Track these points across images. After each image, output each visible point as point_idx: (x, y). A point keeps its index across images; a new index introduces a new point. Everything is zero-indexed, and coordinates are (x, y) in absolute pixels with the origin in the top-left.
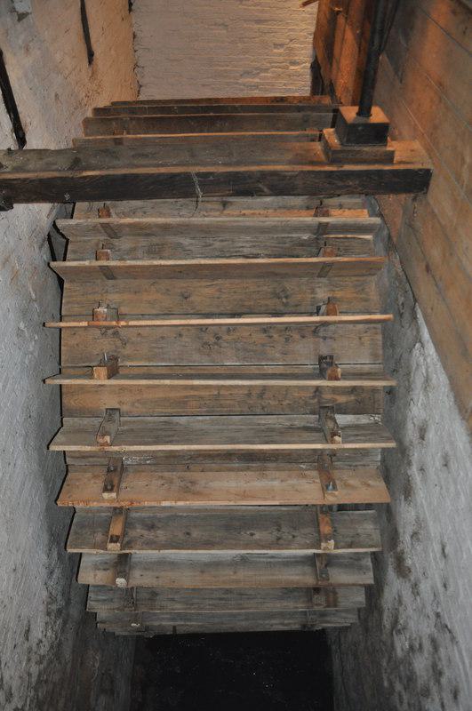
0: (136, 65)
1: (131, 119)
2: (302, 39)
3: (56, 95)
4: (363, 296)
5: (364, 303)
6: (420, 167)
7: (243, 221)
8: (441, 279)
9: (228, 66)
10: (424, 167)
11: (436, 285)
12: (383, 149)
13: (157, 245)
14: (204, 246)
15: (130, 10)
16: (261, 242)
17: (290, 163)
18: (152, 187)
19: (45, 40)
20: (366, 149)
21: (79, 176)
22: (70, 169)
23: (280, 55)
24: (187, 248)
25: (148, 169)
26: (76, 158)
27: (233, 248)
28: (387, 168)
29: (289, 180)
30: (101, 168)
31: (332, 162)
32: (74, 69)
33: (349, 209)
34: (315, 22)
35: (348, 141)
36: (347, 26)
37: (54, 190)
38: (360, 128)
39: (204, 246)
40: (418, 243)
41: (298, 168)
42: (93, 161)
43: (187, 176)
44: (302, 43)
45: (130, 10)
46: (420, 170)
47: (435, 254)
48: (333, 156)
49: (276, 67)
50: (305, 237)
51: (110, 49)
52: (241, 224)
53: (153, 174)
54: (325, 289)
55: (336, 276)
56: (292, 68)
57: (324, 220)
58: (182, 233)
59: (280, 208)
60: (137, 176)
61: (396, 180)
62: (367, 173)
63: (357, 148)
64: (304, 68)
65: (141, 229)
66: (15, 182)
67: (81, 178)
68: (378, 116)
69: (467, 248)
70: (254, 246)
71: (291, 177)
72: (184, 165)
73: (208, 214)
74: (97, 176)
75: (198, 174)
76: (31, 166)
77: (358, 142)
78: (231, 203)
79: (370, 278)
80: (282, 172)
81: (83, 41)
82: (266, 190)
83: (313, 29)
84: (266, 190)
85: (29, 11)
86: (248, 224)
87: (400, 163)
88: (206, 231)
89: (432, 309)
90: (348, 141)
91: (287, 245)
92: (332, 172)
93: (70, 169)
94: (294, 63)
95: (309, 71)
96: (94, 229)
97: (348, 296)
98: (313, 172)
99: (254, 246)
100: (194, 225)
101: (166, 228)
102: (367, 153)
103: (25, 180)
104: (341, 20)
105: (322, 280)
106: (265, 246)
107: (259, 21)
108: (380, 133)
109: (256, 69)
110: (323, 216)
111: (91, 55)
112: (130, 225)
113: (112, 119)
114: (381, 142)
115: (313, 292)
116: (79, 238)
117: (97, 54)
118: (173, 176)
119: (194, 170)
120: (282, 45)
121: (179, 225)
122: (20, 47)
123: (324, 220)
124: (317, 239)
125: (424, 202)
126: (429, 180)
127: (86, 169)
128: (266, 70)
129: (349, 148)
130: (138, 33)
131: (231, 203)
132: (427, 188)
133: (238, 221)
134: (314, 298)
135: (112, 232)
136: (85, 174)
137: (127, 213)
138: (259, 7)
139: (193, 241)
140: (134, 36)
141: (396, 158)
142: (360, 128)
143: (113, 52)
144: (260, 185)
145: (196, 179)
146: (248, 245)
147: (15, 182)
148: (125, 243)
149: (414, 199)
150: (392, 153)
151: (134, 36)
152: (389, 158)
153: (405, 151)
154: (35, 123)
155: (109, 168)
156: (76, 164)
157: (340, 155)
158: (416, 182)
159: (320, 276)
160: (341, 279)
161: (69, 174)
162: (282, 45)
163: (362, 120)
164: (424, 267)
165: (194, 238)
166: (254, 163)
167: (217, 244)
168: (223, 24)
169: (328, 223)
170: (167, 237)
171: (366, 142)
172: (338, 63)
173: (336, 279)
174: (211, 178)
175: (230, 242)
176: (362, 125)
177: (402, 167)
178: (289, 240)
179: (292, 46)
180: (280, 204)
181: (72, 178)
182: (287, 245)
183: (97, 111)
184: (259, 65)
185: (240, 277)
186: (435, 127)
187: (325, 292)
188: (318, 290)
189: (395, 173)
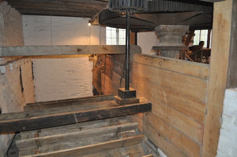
0: (35, 96)
1: (42, 105)
2: (89, 84)
3: (12, 100)
4: (138, 151)
5: (139, 154)
6: (148, 103)
7: (91, 131)
8: (166, 136)
9: (66, 93)
10: (149, 103)
11: (165, 139)
12: (135, 99)
13: (58, 146)
14: (76, 144)
15: (33, 79)
16: (97, 139)
17: (107, 107)
18: (58, 121)
19: (9, 82)
20: (130, 99)
21: (30, 119)
22: (25, 117)
23: (83, 89)
24: (70, 146)
25: (56, 114)
26: (89, 61)
27: (87, 143)
28: (138, 104)
29: (108, 112)
30: (38, 116)
31: (121, 105)
32: (17, 93)
33: (124, 124)
34: (92, 78)
35: (125, 97)
36: (106, 76)
37: (18, 126)
38: (128, 93)
39: (76, 144)
40: (153, 128)
41: (110, 108)
42: (34, 114)
43: (72, 115)
44: (89, 85)
45: (33, 79)
46: (148, 104)
47: (162, 129)
48: (122, 103)
49: (82, 92)
50: (112, 135)
51: (28, 89)
52: (90, 132)
53: (59, 116)
54: (125, 151)
55: (127, 146)
56: (87, 92)
57: (120, 126)
58: (67, 140)
59: (100, 127)
60: (52, 117)
61: (141, 108)
62: (133, 107)
63: (127, 99)
64: (91, 91)
65: (52, 140)
66: (2, 124)
67: (30, 120)
68: (131, 89)
69: (174, 122)
70: (95, 141)
71: (108, 111)
72: (70, 111)
73: (74, 132)
74: (37, 119)
75: (76, 114)
76: (9, 118)
77: (127, 97)
78: (83, 128)
79: (138, 145)
80: (105, 110)
81: (20, 85)
82: (100, 117)
83: (92, 80)
84: (100, 117)
85: (5, 73)
86: (93, 132)
87: (141, 102)
88: (76, 138)
89: (166, 148)
90: (125, 97)
91: (107, 139)
92: (121, 108)
93: (25, 117)
94: (87, 91)
95: (92, 92)
96: (32, 143)
97: (133, 152)
98: (115, 108)
99: (95, 141)
100: (73, 135)
101: (61, 139)
102: (131, 100)
103: (6, 123)
104: (103, 75)
105: (123, 148)
106: (99, 140)
107: (75, 80)
108: (134, 94)
109: (76, 93)
110: (119, 125)
111: (23, 89)
112: (47, 139)
113: (35, 106)
114: (134, 97)
115: (120, 154)
116: (24, 149)
117: (24, 90)
118: (66, 116)
119: (74, 113)
120: (83, 86)
121: (67, 136)
122: (2, 83)
123: (120, 126)
124: (116, 135)
125: (151, 114)
126: (151, 106)
127: (32, 117)
128: (79, 93)
129: (126, 100)
130: (36, 86)
131: (83, 128)
132: (151, 109)
133: (89, 131)
134: (121, 156)
135: (39, 144)
136: (32, 118)
137: (46, 135)
138: (75, 76)
139: (72, 143)
140: (34, 87)
141: (140, 102)
142: (128, 93)
143: (28, 90)
144: (98, 115)
145: (75, 116)
146: (93, 141)
147: (2, 124)
148: (44, 148)
149: (147, 114)
150: (139, 100)
151: (34, 87)
152: (138, 101)
153: (142, 99)
154: (4, 109)
155: (41, 115)
156: (27, 115)
157: (123, 102)
158: (147, 108)
159: (122, 147)
160: (129, 146)
161: (25, 119)
162: (83, 86)
163: (127, 91)
164: (157, 135)
165: (71, 142)
166: (95, 108)
167: (81, 143)
168: (64, 81)
169: (121, 127)
170: (61, 143)
171: (130, 97)
172: (104, 87)
173: (127, 147)
174: (81, 115)
175: (86, 141)
176: (128, 92)
177: (142, 103)
178: (106, 137)
179: (86, 86)
180: (100, 126)
181: (27, 120)
182: (107, 139)
183: (27, 104)
184: (76, 92)
185: (93, 153)
186: (149, 91)
187: (124, 153)
188: (122, 152)
189: (141, 106)
